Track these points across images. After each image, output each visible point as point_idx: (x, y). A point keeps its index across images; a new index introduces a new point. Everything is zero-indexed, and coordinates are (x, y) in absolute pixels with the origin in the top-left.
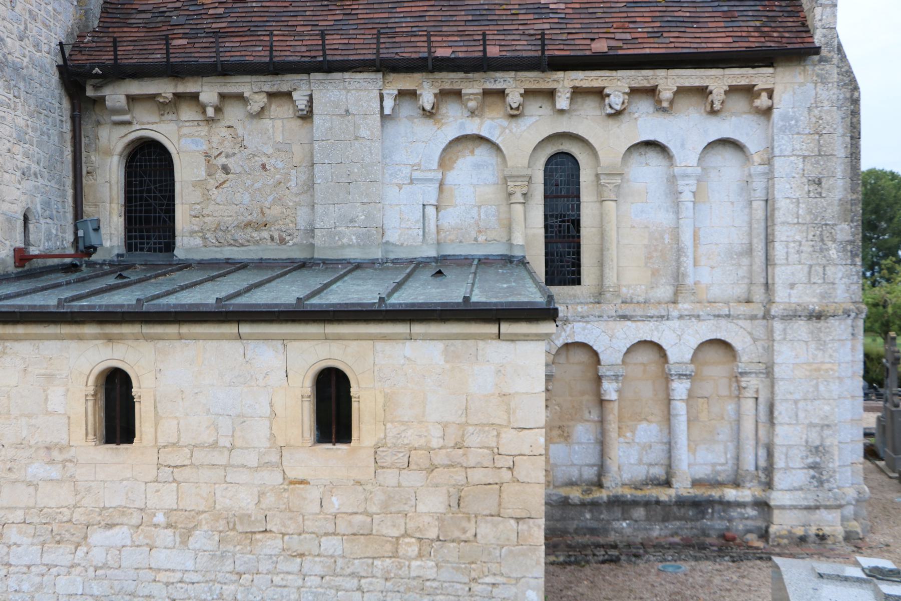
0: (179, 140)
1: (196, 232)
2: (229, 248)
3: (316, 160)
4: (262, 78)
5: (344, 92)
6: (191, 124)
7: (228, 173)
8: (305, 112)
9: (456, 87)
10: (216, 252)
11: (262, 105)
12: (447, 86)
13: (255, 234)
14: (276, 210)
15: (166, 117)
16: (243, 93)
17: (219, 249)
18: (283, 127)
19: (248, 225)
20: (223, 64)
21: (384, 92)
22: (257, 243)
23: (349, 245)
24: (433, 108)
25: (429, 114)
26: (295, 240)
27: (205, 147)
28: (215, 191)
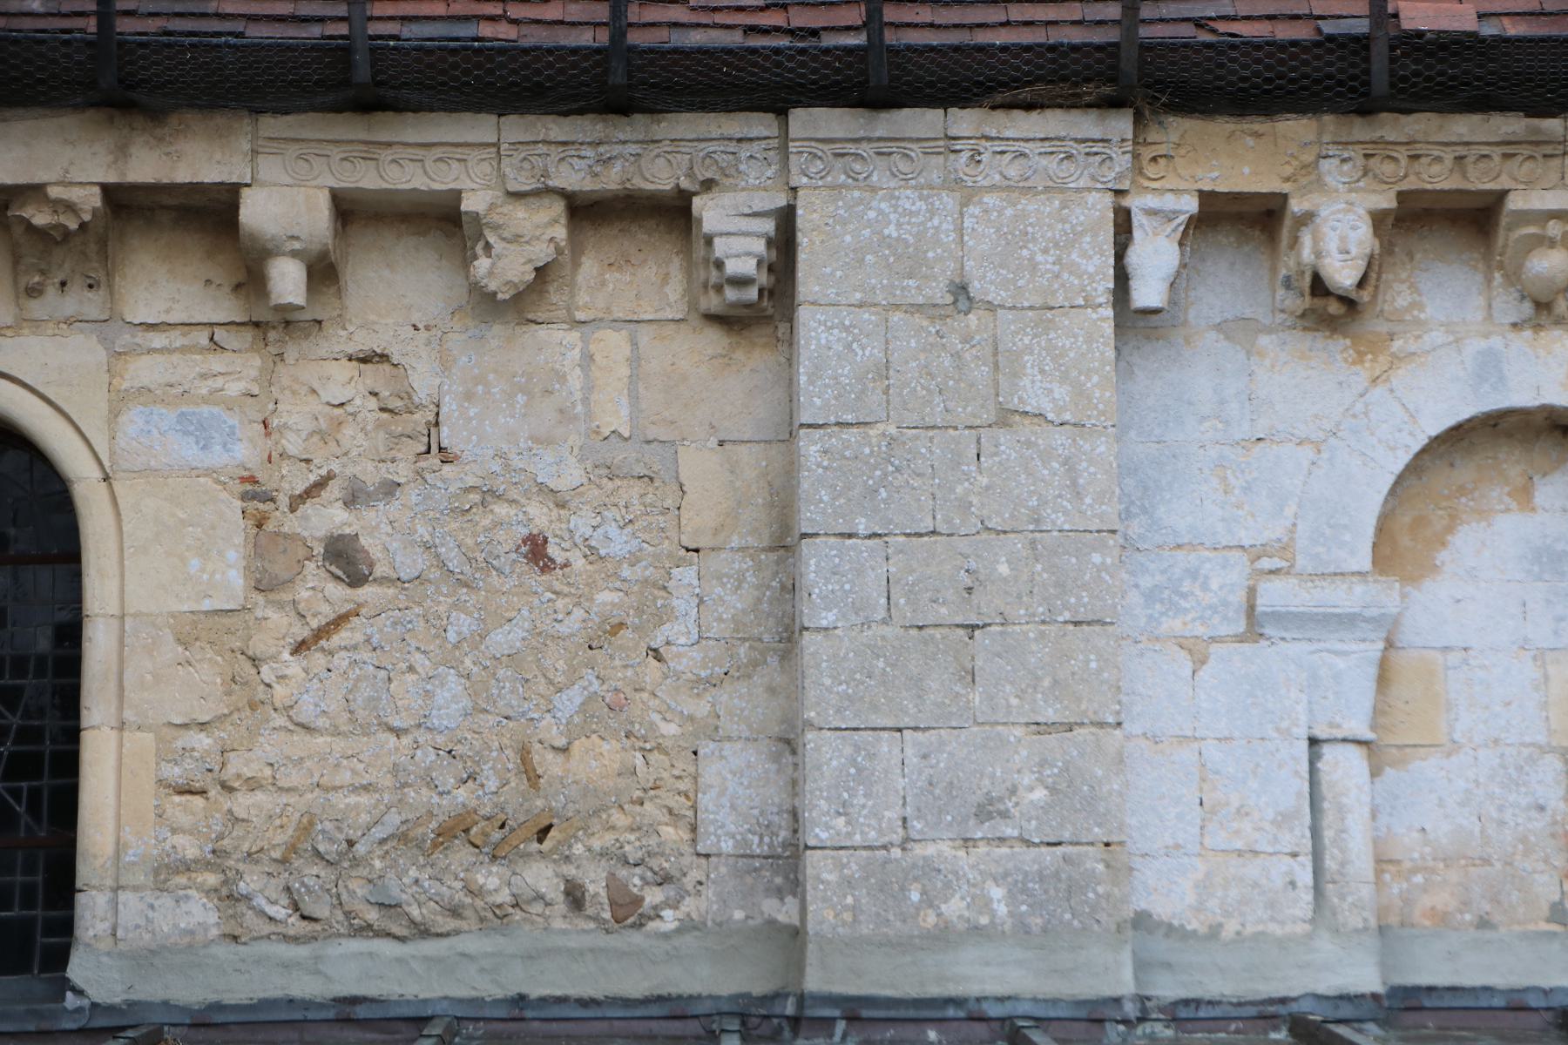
0: (114, 414)
1: (187, 867)
2: (356, 945)
3: (809, 517)
4: (556, 128)
5: (948, 201)
6: (176, 339)
7: (356, 579)
8: (752, 294)
9: (1479, 181)
10: (286, 966)
11: (542, 253)
12: (1438, 177)
13: (490, 878)
14: (598, 760)
15: (52, 303)
16: (457, 195)
17: (302, 951)
18: (635, 361)
19: (457, 829)
20: (380, 51)
21: (1134, 203)
22: (498, 918)
23: (976, 929)
24: (1361, 284)
25: (1331, 309)
26: (689, 905)
27: (245, 452)
28: (294, 667)
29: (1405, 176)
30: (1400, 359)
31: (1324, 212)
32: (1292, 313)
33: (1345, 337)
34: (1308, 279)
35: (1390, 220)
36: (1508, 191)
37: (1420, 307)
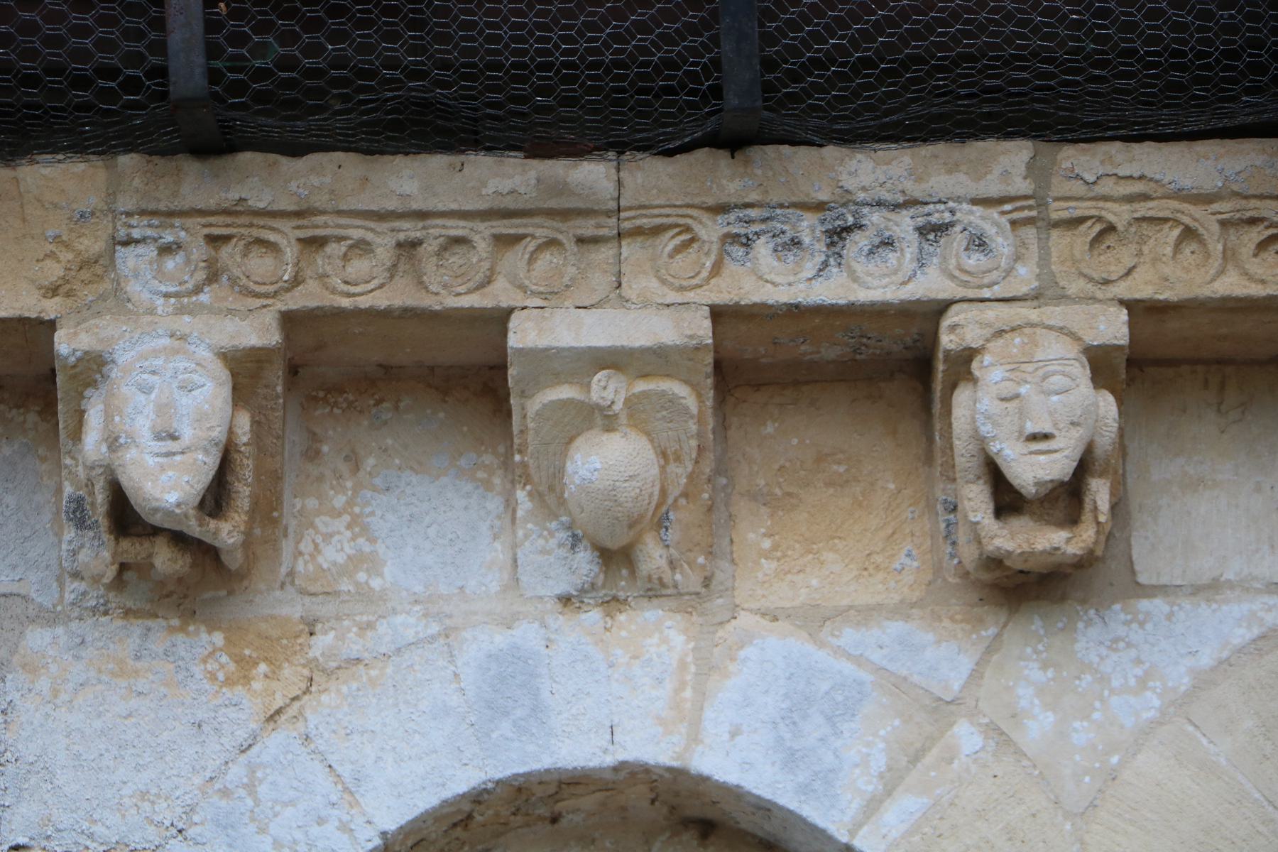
9: (449, 289)
12: (361, 282)
24: (216, 498)
25: (180, 568)
29: (296, 281)
30: (328, 673)
31: (124, 356)
32: (96, 580)
33: (210, 631)
34: (101, 497)
35: (276, 378)
36: (510, 311)
37: (371, 563)
